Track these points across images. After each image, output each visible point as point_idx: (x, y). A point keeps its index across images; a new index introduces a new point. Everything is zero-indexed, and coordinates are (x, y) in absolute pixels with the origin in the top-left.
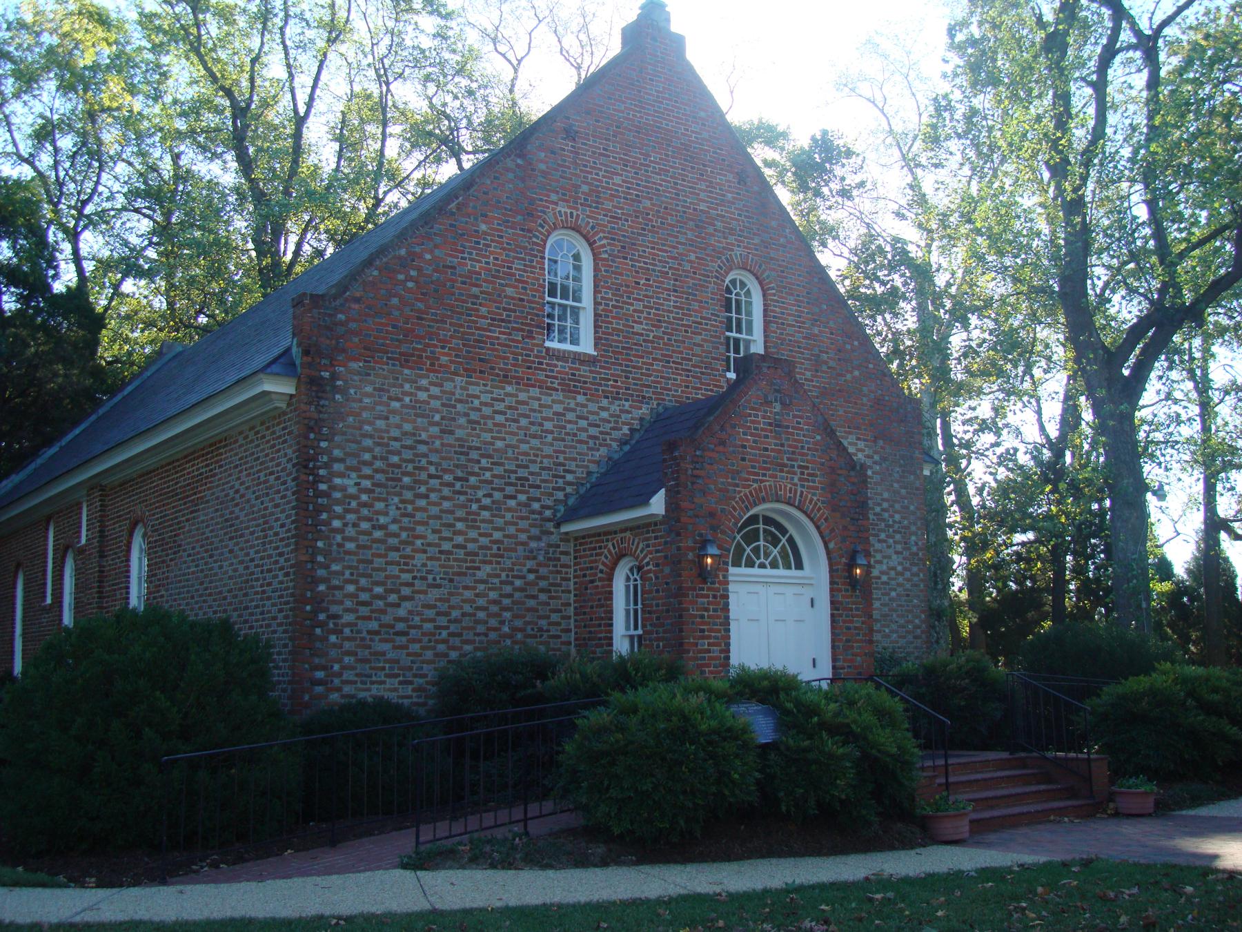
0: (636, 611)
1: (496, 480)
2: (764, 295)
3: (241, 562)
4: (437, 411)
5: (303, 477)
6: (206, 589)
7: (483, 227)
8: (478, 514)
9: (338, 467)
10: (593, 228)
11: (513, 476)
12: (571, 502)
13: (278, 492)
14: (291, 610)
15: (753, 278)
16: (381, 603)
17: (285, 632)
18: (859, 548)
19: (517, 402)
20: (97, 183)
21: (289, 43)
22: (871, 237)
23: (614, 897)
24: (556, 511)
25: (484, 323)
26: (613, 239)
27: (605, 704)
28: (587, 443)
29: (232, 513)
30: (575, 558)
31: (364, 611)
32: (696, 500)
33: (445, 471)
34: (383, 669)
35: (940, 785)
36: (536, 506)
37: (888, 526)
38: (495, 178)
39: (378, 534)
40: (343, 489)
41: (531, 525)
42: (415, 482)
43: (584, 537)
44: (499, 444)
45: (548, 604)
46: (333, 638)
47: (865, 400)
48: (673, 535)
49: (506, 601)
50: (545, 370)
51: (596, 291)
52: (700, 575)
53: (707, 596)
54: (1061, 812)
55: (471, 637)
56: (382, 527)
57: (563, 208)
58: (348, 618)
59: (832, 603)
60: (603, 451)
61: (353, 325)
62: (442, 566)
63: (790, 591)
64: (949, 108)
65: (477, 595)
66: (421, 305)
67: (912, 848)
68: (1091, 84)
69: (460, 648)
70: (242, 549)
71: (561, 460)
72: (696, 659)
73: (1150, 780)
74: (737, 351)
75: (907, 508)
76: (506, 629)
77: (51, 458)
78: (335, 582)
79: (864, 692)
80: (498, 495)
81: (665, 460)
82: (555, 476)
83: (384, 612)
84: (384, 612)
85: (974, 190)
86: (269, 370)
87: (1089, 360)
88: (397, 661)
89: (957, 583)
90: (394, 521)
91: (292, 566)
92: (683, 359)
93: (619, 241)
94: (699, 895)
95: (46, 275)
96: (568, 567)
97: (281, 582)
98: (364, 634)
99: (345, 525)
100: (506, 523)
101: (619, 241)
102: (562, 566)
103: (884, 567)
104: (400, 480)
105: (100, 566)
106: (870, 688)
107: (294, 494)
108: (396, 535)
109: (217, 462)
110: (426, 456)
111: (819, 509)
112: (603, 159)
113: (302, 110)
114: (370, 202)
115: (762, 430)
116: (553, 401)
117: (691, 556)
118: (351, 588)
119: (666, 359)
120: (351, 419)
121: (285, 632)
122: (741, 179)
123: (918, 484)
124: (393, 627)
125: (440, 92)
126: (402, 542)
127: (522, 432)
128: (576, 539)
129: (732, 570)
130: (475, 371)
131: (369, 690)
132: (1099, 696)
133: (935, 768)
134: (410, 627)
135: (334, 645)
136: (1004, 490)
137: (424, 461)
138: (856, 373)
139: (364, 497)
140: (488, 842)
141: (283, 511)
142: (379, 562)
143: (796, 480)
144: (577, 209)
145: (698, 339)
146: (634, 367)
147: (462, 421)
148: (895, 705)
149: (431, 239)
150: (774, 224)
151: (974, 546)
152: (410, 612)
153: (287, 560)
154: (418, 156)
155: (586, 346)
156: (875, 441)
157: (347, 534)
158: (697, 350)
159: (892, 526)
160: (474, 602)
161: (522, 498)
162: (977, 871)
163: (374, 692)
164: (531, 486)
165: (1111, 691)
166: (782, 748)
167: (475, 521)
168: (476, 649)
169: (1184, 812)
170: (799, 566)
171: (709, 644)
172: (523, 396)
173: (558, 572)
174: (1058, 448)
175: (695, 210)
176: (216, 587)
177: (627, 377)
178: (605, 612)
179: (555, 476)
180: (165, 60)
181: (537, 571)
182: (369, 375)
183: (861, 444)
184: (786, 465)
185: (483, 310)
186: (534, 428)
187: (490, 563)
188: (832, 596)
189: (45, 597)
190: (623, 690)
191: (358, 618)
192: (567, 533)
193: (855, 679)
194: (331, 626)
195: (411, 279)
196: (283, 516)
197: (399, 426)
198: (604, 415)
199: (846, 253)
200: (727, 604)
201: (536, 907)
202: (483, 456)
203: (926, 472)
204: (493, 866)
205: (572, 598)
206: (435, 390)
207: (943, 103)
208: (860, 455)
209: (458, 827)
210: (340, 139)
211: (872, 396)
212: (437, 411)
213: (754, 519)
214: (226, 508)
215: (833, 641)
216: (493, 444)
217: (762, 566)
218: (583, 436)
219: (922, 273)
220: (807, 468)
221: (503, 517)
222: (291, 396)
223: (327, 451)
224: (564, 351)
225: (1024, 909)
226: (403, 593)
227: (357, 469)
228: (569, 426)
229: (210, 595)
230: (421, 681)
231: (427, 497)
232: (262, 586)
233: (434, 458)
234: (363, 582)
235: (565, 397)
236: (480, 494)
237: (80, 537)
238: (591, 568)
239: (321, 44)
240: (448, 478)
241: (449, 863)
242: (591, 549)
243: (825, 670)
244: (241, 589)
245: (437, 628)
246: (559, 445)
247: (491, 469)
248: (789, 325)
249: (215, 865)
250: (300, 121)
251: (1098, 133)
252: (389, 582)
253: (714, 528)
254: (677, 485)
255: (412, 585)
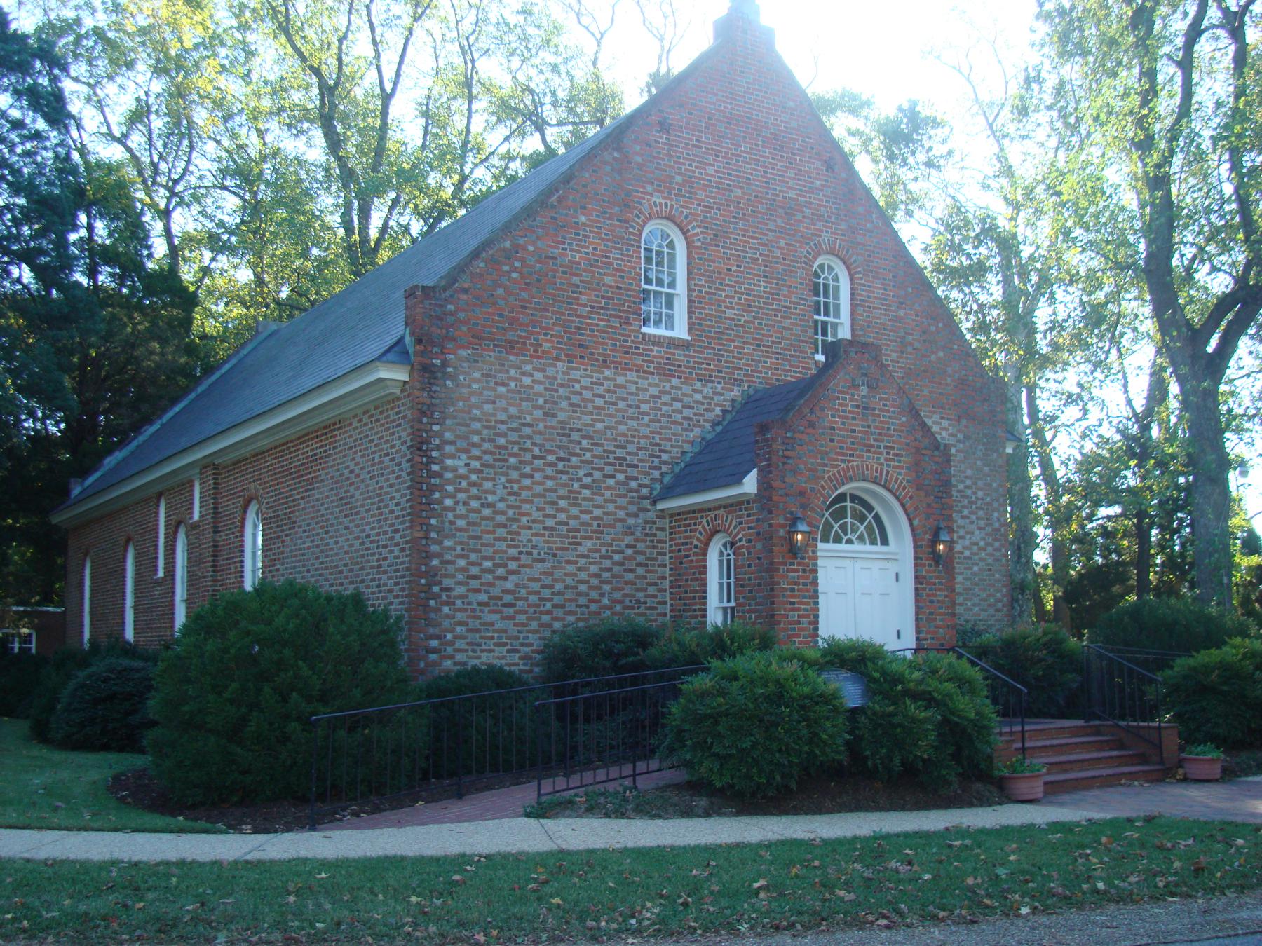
0: (729, 585)
1: (596, 460)
2: (851, 280)
3: (357, 538)
4: (541, 395)
5: (417, 459)
6: (322, 563)
7: (583, 219)
8: (580, 493)
9: (449, 449)
10: (686, 217)
11: (612, 456)
12: (667, 480)
13: (393, 472)
14: (407, 583)
15: (841, 264)
16: (490, 577)
17: (401, 603)
18: (942, 525)
19: (616, 386)
20: (188, 162)
21: (374, 20)
22: (957, 208)
23: (719, 842)
24: (652, 489)
25: (584, 310)
26: (706, 228)
27: (707, 670)
28: (681, 424)
29: (346, 492)
30: (671, 534)
31: (474, 584)
32: (787, 480)
33: (548, 452)
34: (492, 638)
35: (1016, 749)
36: (633, 484)
37: (971, 503)
38: (594, 171)
39: (487, 512)
40: (454, 470)
41: (630, 503)
42: (521, 462)
43: (679, 514)
44: (599, 426)
45: (645, 577)
46: (446, 609)
47: (949, 380)
48: (765, 513)
49: (606, 575)
50: (641, 355)
51: (690, 278)
52: (790, 551)
53: (797, 571)
54: (1132, 776)
55: (573, 608)
56: (490, 505)
57: (657, 199)
58: (460, 590)
59: (916, 577)
60: (697, 431)
61: (461, 315)
62: (547, 542)
63: (876, 566)
64: (1038, 79)
65: (579, 569)
66: (524, 295)
67: (990, 806)
68: (1179, 64)
69: (563, 619)
70: (357, 526)
71: (657, 440)
72: (786, 630)
73: (1218, 748)
74: (825, 333)
75: (990, 485)
76: (605, 601)
77: (152, 435)
78: (448, 557)
79: (946, 662)
80: (597, 474)
81: (757, 442)
82: (651, 456)
83: (491, 584)
84: (491, 584)
85: (1061, 164)
86: (384, 359)
87: (1172, 338)
88: (505, 631)
89: (1041, 556)
90: (502, 500)
91: (407, 542)
92: (773, 342)
93: (712, 229)
94: (795, 840)
95: (141, 255)
96: (665, 542)
97: (397, 557)
98: (475, 606)
99: (457, 503)
100: (606, 501)
101: (712, 229)
102: (658, 541)
103: (967, 543)
104: (506, 461)
105: (215, 541)
106: (951, 658)
107: (408, 474)
108: (503, 513)
109: (331, 443)
110: (530, 437)
111: (904, 488)
112: (696, 151)
113: (388, 88)
114: (456, 178)
115: (850, 412)
116: (650, 385)
117: (782, 532)
118: (462, 563)
119: (757, 343)
120: (461, 404)
121: (401, 603)
122: (829, 167)
123: (1000, 461)
124: (500, 599)
125: (524, 66)
126: (508, 519)
127: (620, 415)
128: (671, 516)
129: (821, 546)
130: (575, 357)
131: (479, 658)
132: (1172, 668)
133: (1011, 733)
134: (516, 599)
135: (447, 616)
136: (1087, 464)
137: (529, 443)
138: (941, 354)
139: (474, 477)
140: (602, 794)
141: (398, 491)
142: (488, 538)
143: (882, 460)
144: (671, 200)
145: (787, 323)
146: (726, 351)
147: (564, 404)
148: (975, 674)
149: (534, 232)
150: (861, 209)
151: (1059, 519)
152: (517, 585)
153: (401, 537)
154: (503, 131)
155: (680, 331)
156: (959, 421)
157: (458, 512)
158: (787, 334)
159: (975, 503)
160: (576, 575)
161: (621, 477)
162: (1047, 824)
163: (484, 660)
164: (629, 466)
165: (1182, 664)
166: (869, 713)
167: (576, 499)
168: (578, 620)
169: (1250, 779)
170: (885, 542)
171: (799, 616)
172: (620, 380)
173: (654, 547)
174: (1144, 420)
175: (784, 197)
176: (332, 561)
177: (719, 361)
178: (700, 585)
179: (651, 456)
180: (250, 37)
181: (634, 546)
182: (477, 361)
183: (945, 423)
184: (872, 446)
185: (583, 298)
186: (631, 411)
187: (591, 538)
188: (916, 571)
189: (156, 570)
190: (721, 658)
191: (468, 591)
192: (662, 510)
193: (938, 650)
194: (444, 598)
195: (515, 269)
196: (397, 495)
197: (505, 410)
198: (698, 397)
199: (932, 224)
200: (816, 578)
201: (651, 849)
202: (584, 437)
203: (1009, 450)
204: (607, 816)
205: (668, 572)
206: (539, 376)
207: (1032, 74)
208: (944, 434)
209: (575, 780)
210: (426, 114)
211: (956, 376)
212: (541, 395)
213: (841, 497)
214: (341, 487)
215: (917, 614)
216: (592, 426)
217: (849, 542)
218: (678, 417)
219: (1008, 245)
220: (893, 448)
221: (603, 495)
222: (405, 382)
223: (439, 434)
224: (660, 337)
225: (1088, 855)
226: (510, 567)
227: (467, 451)
228: (664, 408)
229: (326, 568)
230: (527, 649)
231: (532, 476)
232: (378, 560)
233: (538, 439)
234: (473, 557)
235: (660, 380)
236: (581, 473)
237: (192, 513)
238: (686, 544)
239: (407, 21)
240: (551, 458)
241: (567, 813)
242: (685, 525)
243: (909, 641)
244: (357, 563)
245: (541, 599)
246: (655, 427)
247: (591, 450)
248: (875, 308)
249: (356, 814)
250: (387, 98)
251: (1185, 110)
252: (497, 556)
253: (804, 506)
254: (769, 466)
255: (518, 559)
